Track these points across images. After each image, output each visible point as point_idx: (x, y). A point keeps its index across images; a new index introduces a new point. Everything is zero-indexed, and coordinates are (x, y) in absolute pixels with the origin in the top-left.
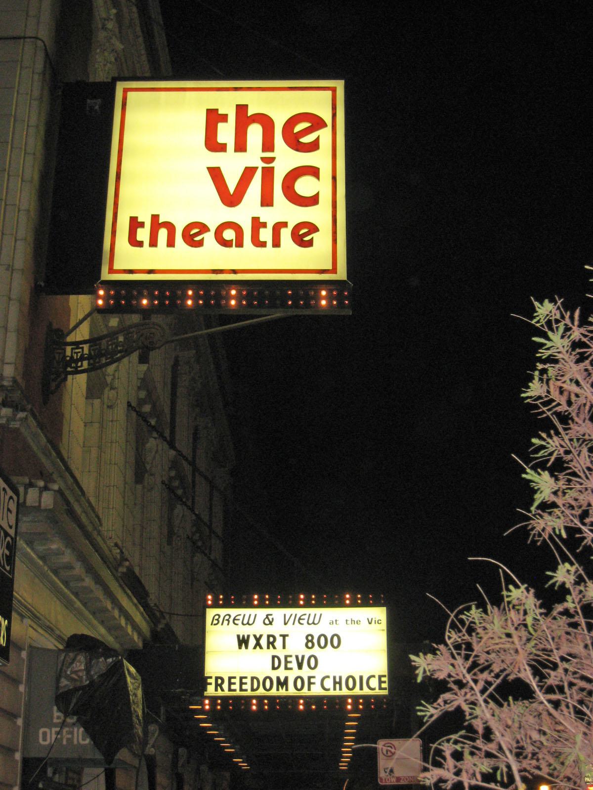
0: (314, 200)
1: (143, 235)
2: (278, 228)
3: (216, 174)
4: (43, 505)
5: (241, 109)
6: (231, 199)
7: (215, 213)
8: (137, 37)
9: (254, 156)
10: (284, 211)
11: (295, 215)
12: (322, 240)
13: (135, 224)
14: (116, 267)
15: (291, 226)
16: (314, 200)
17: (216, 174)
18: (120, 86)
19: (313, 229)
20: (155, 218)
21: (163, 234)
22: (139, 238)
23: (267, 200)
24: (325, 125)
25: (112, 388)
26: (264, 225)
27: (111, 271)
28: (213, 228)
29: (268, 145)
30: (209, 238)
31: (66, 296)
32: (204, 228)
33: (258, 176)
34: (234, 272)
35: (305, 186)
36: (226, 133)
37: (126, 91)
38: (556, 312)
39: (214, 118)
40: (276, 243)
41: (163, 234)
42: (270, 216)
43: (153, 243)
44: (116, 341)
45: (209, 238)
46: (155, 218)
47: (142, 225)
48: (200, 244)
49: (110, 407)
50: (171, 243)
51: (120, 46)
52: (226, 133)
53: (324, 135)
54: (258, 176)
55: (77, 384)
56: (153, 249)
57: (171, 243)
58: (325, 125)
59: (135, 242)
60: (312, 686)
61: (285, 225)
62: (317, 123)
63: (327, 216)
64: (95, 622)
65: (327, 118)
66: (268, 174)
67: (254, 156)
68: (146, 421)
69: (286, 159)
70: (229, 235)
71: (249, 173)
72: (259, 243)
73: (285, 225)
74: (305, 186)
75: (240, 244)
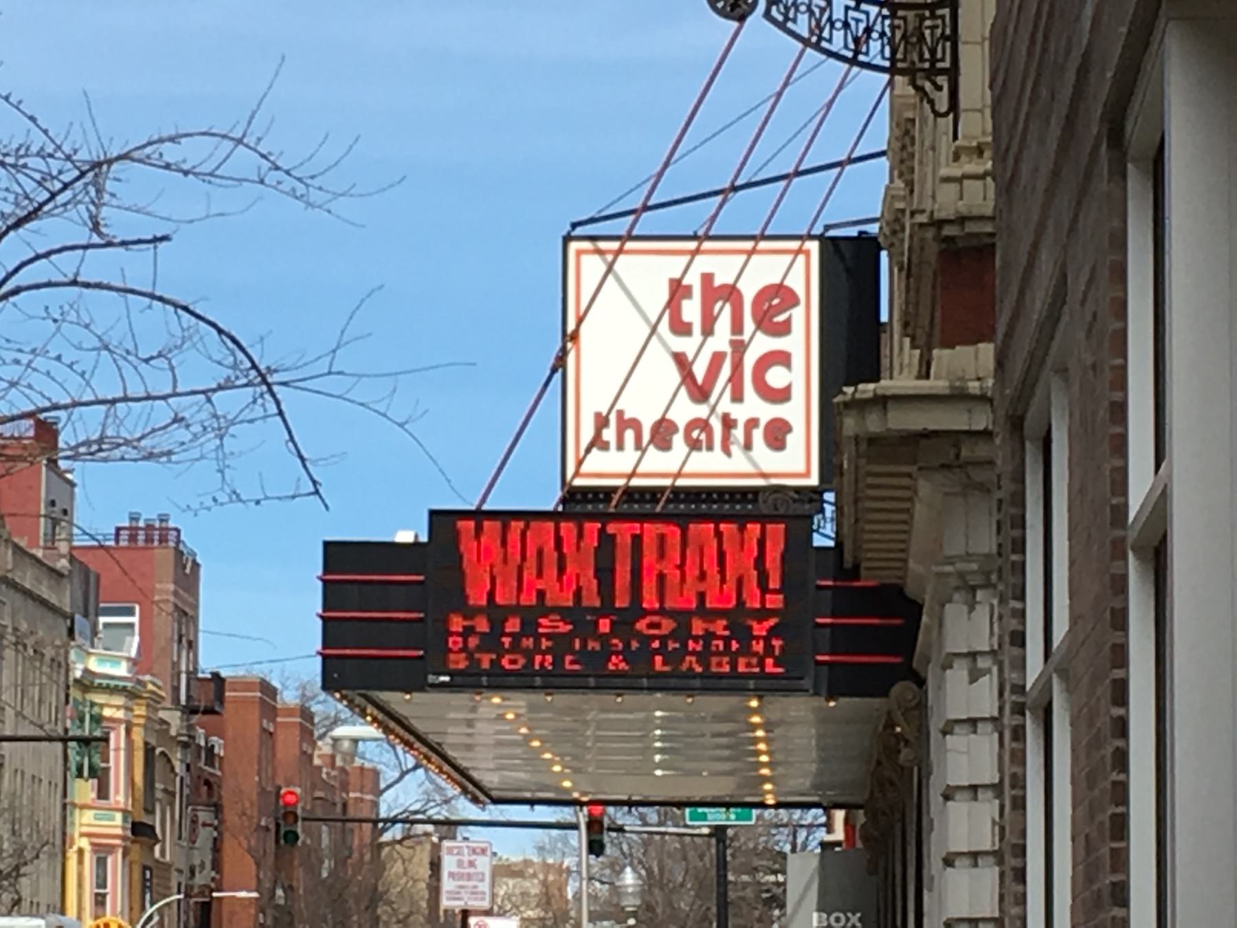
2: (752, 423)
4: (989, 775)
6: (700, 393)
10: (754, 407)
12: (795, 440)
15: (763, 424)
23: (738, 397)
29: (737, 327)
35: (776, 377)
36: (691, 310)
38: (459, 838)
39: (678, 290)
41: (629, 435)
44: (671, 885)
52: (691, 310)
56: (620, 453)
60: (21, 107)
63: (802, 413)
71: (717, 358)
74: (776, 377)
75: (710, 448)
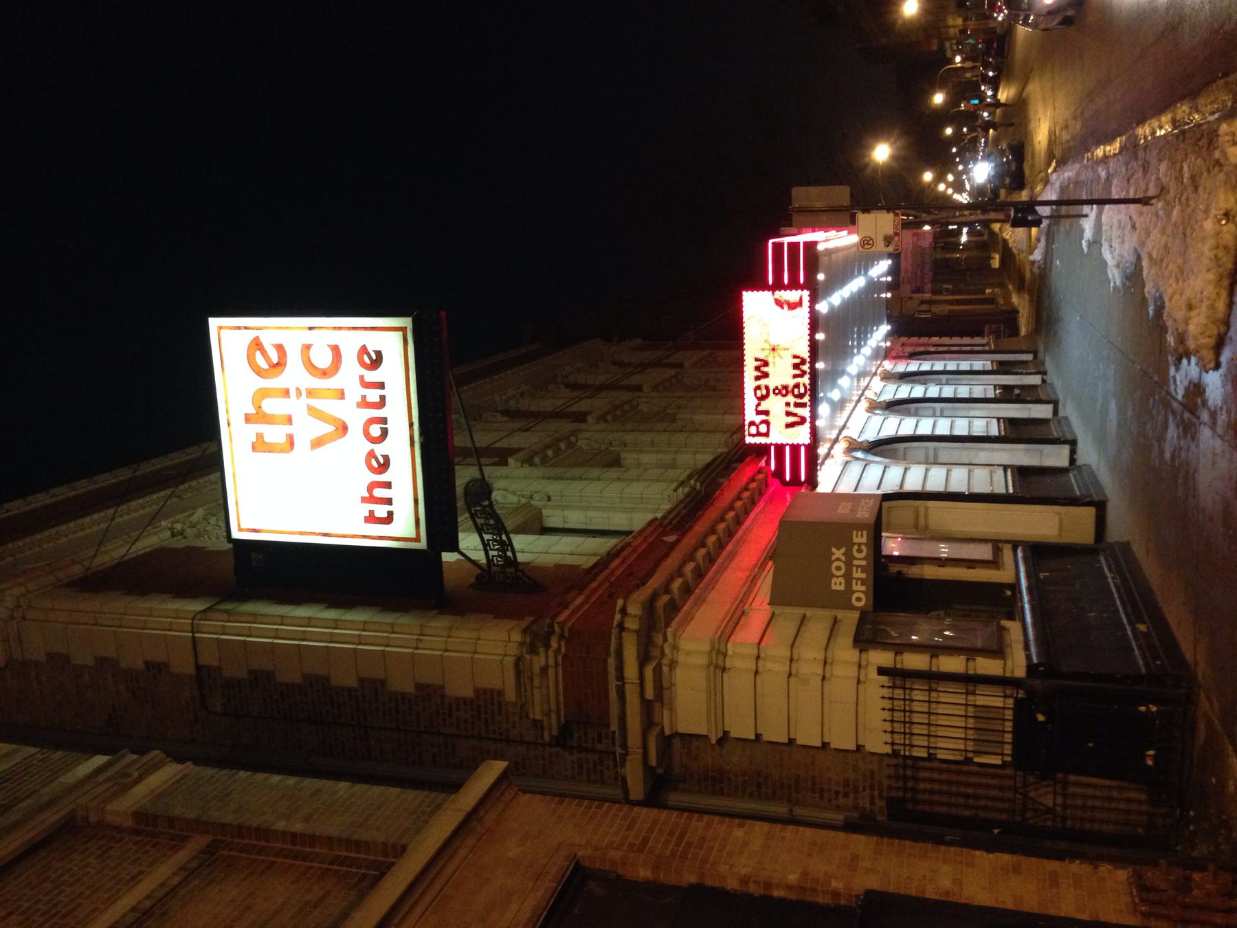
0: (336, 350)
1: (381, 511)
3: (317, 443)
5: (248, 419)
7: (356, 445)
8: (190, 487)
9: (296, 407)
11: (351, 369)
12: (375, 341)
13: (371, 518)
14: (413, 535)
16: (336, 350)
17: (317, 443)
18: (236, 534)
19: (364, 350)
20: (364, 500)
21: (379, 493)
22: (385, 515)
24: (257, 338)
25: (531, 497)
26: (364, 397)
27: (417, 539)
28: (370, 446)
30: (380, 450)
31: (444, 566)
32: (371, 454)
33: (317, 403)
34: (411, 425)
36: (274, 434)
37: (240, 530)
39: (260, 445)
40: (381, 386)
41: (379, 493)
42: (355, 392)
43: (389, 501)
45: (380, 450)
46: (364, 500)
47: (372, 512)
48: (386, 458)
49: (549, 499)
50: (388, 485)
51: (200, 512)
52: (274, 434)
53: (268, 340)
54: (317, 403)
55: (527, 547)
57: (388, 485)
58: (257, 338)
59: (389, 519)
61: (362, 378)
62: (257, 344)
64: (740, 532)
65: (251, 335)
66: (311, 393)
67: (296, 407)
68: (561, 457)
69: (295, 375)
70: (375, 431)
71: (313, 412)
72: (382, 403)
73: (362, 378)
74: (323, 359)
75: (384, 420)
